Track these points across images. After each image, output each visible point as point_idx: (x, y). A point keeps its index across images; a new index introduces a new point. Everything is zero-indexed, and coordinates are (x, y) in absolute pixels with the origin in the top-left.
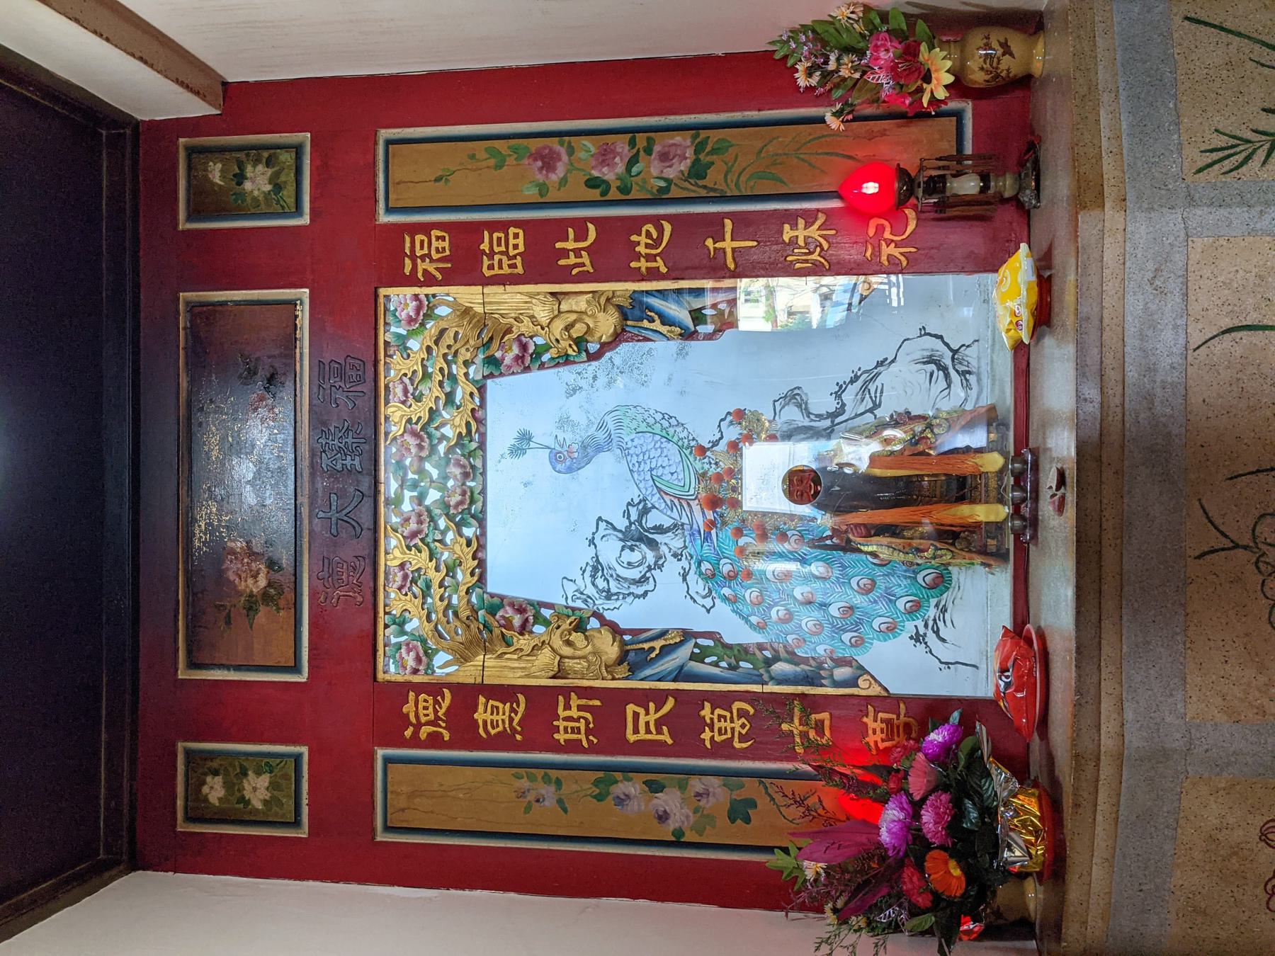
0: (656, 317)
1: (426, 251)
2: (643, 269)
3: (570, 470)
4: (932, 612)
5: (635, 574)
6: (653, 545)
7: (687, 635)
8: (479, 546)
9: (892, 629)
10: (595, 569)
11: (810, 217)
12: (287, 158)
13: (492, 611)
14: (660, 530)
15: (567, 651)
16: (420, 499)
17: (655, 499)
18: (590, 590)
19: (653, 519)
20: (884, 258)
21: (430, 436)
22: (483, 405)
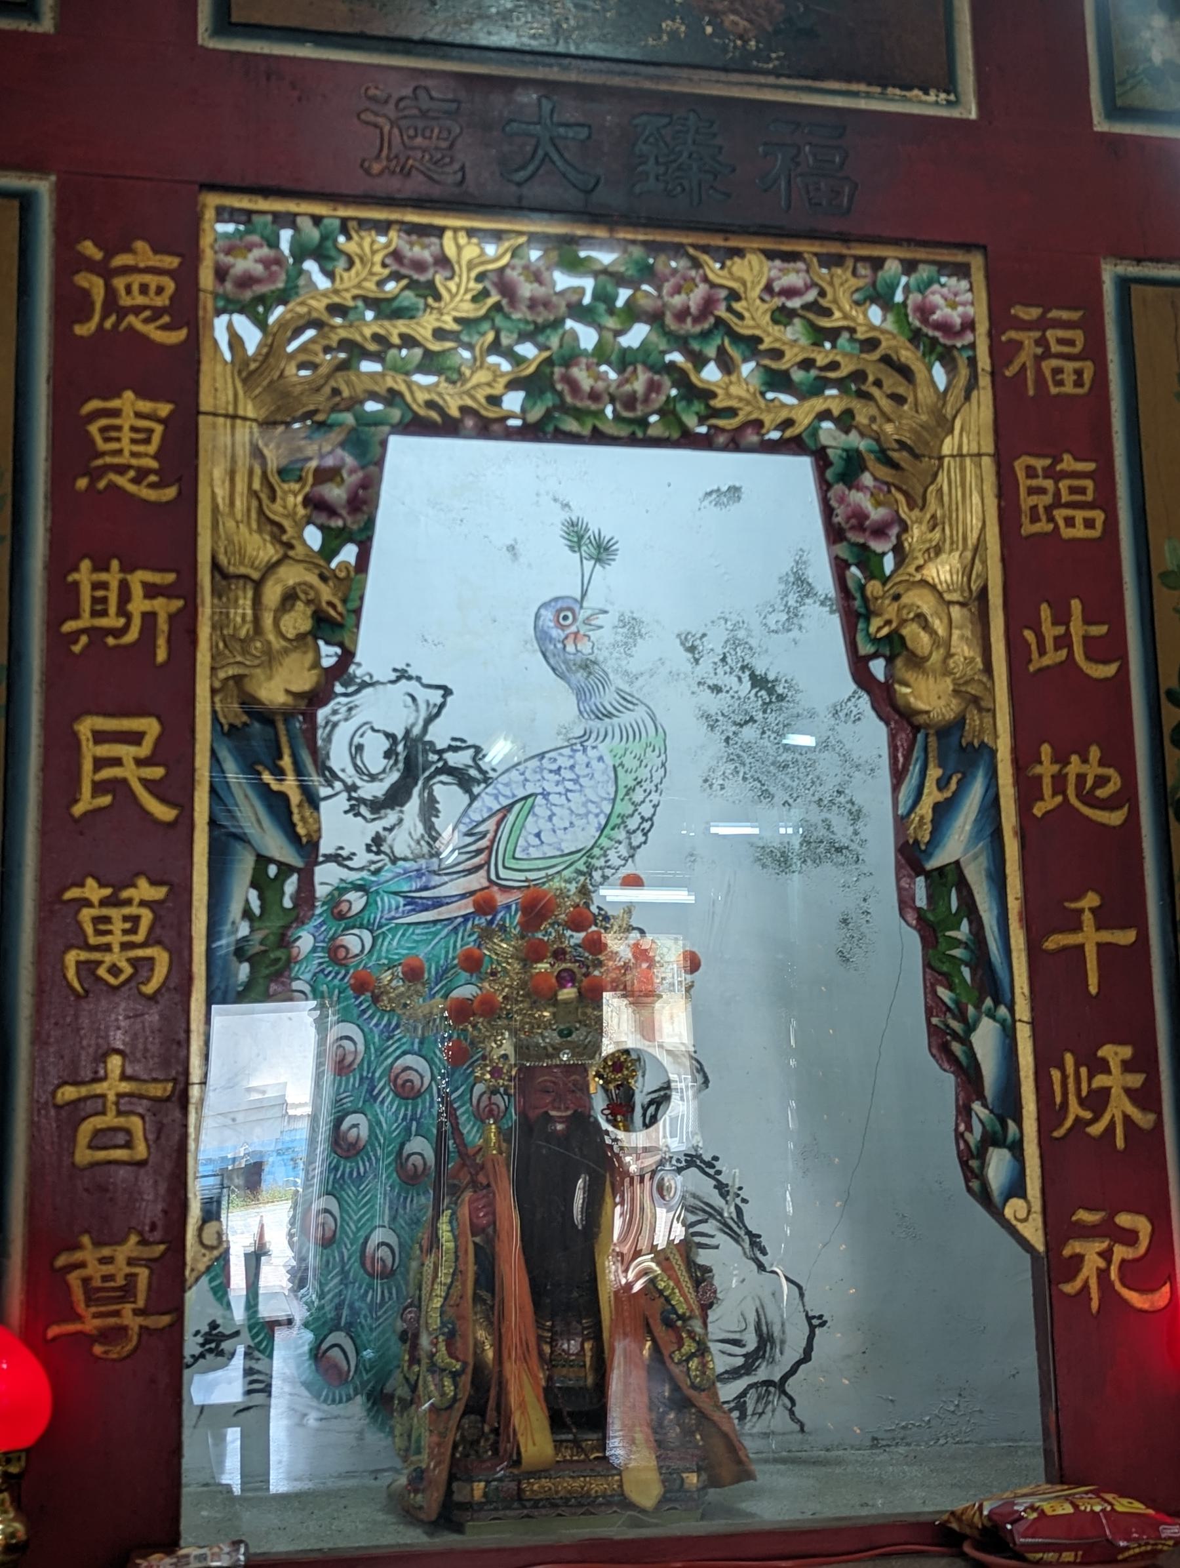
1: (1055, 348)
2: (1038, 770)
3: (542, 637)
6: (396, 797)
14: (430, 809)
17: (488, 801)
20: (1013, 334)
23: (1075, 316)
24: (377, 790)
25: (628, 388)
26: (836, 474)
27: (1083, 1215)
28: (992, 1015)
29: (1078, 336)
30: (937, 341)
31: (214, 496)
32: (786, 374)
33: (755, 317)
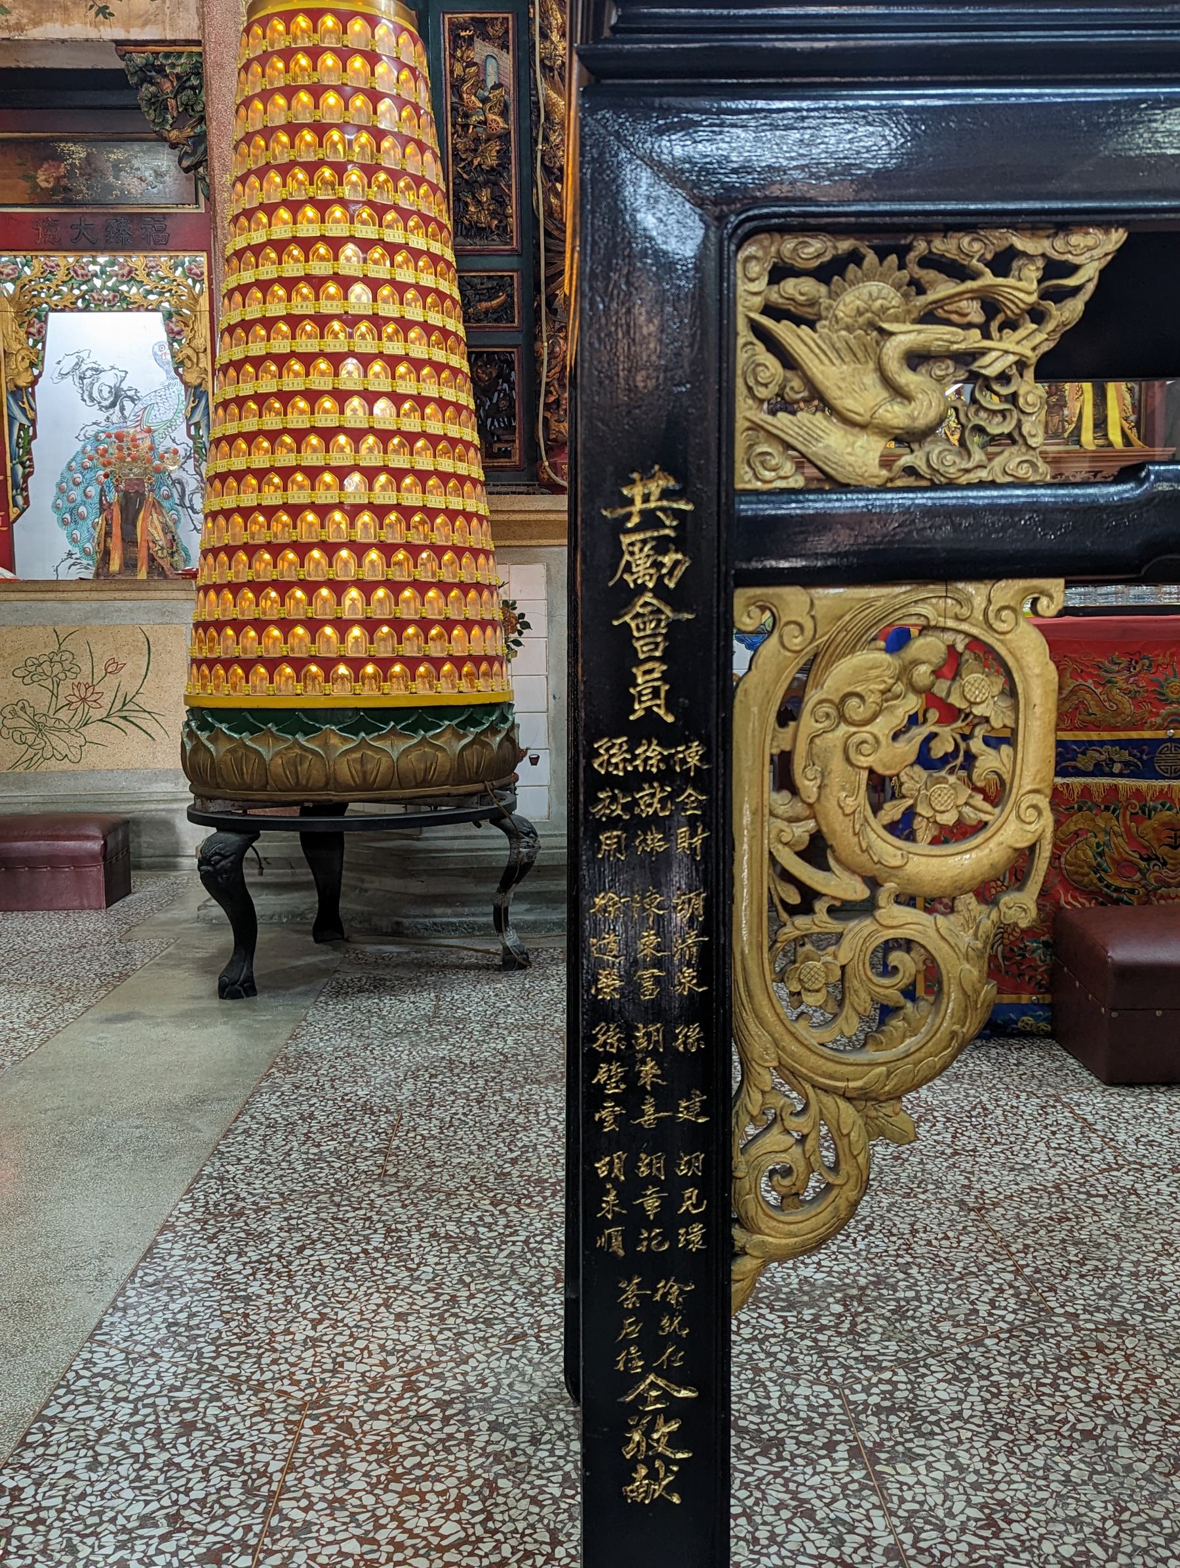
3: (155, 354)
4: (85, 562)
5: (95, 394)
6: (113, 405)
7: (33, 422)
8: (73, 308)
9: (74, 541)
10: (97, 370)
13: (37, 316)
14: (122, 409)
16: (95, 275)
17: (140, 406)
18: (84, 367)
19: (128, 404)
22: (147, 310)
24: (107, 403)
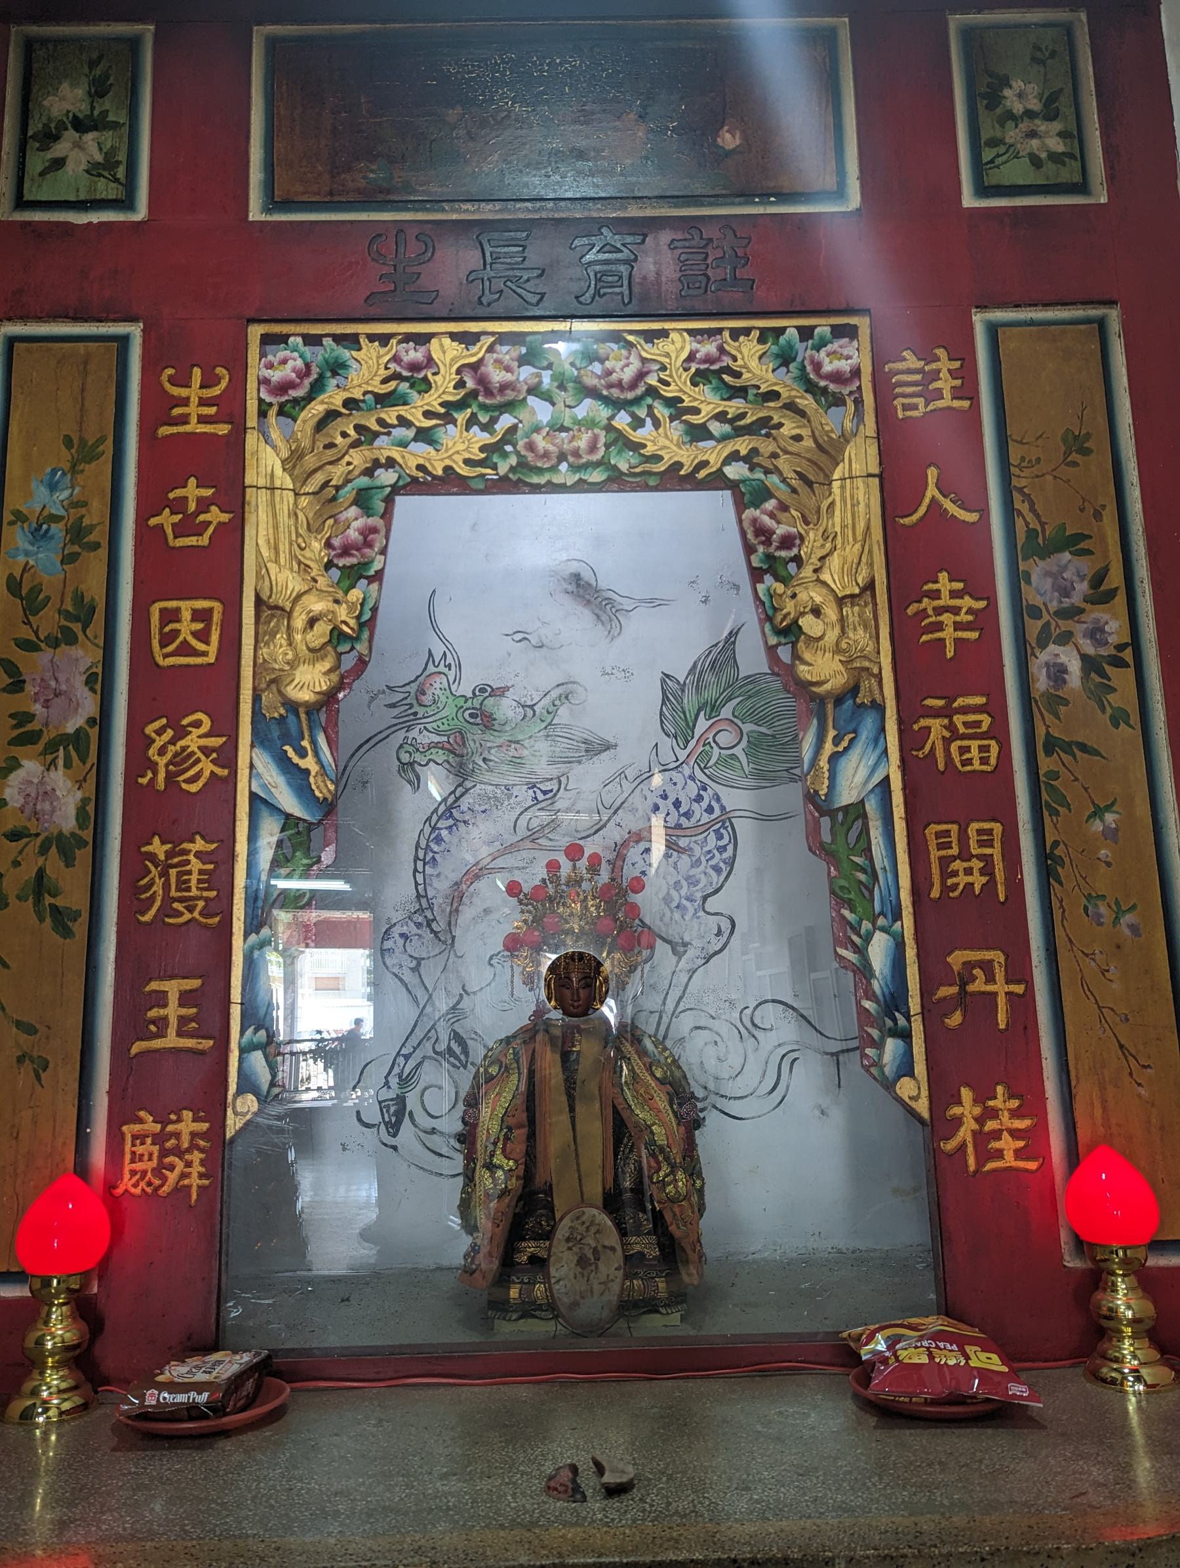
0: (840, 749)
1: (962, 730)
2: (956, 1110)
11: (967, 390)
12: (1069, 173)
15: (299, 622)
20: (924, 722)
21: (637, 401)
23: (980, 700)
25: (575, 444)
26: (746, 497)
27: (930, 702)
28: (883, 930)
29: (986, 720)
30: (827, 391)
31: (259, 552)
32: (703, 427)
33: (680, 385)
